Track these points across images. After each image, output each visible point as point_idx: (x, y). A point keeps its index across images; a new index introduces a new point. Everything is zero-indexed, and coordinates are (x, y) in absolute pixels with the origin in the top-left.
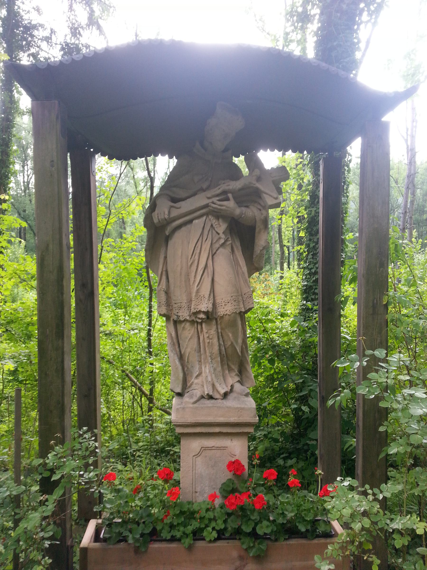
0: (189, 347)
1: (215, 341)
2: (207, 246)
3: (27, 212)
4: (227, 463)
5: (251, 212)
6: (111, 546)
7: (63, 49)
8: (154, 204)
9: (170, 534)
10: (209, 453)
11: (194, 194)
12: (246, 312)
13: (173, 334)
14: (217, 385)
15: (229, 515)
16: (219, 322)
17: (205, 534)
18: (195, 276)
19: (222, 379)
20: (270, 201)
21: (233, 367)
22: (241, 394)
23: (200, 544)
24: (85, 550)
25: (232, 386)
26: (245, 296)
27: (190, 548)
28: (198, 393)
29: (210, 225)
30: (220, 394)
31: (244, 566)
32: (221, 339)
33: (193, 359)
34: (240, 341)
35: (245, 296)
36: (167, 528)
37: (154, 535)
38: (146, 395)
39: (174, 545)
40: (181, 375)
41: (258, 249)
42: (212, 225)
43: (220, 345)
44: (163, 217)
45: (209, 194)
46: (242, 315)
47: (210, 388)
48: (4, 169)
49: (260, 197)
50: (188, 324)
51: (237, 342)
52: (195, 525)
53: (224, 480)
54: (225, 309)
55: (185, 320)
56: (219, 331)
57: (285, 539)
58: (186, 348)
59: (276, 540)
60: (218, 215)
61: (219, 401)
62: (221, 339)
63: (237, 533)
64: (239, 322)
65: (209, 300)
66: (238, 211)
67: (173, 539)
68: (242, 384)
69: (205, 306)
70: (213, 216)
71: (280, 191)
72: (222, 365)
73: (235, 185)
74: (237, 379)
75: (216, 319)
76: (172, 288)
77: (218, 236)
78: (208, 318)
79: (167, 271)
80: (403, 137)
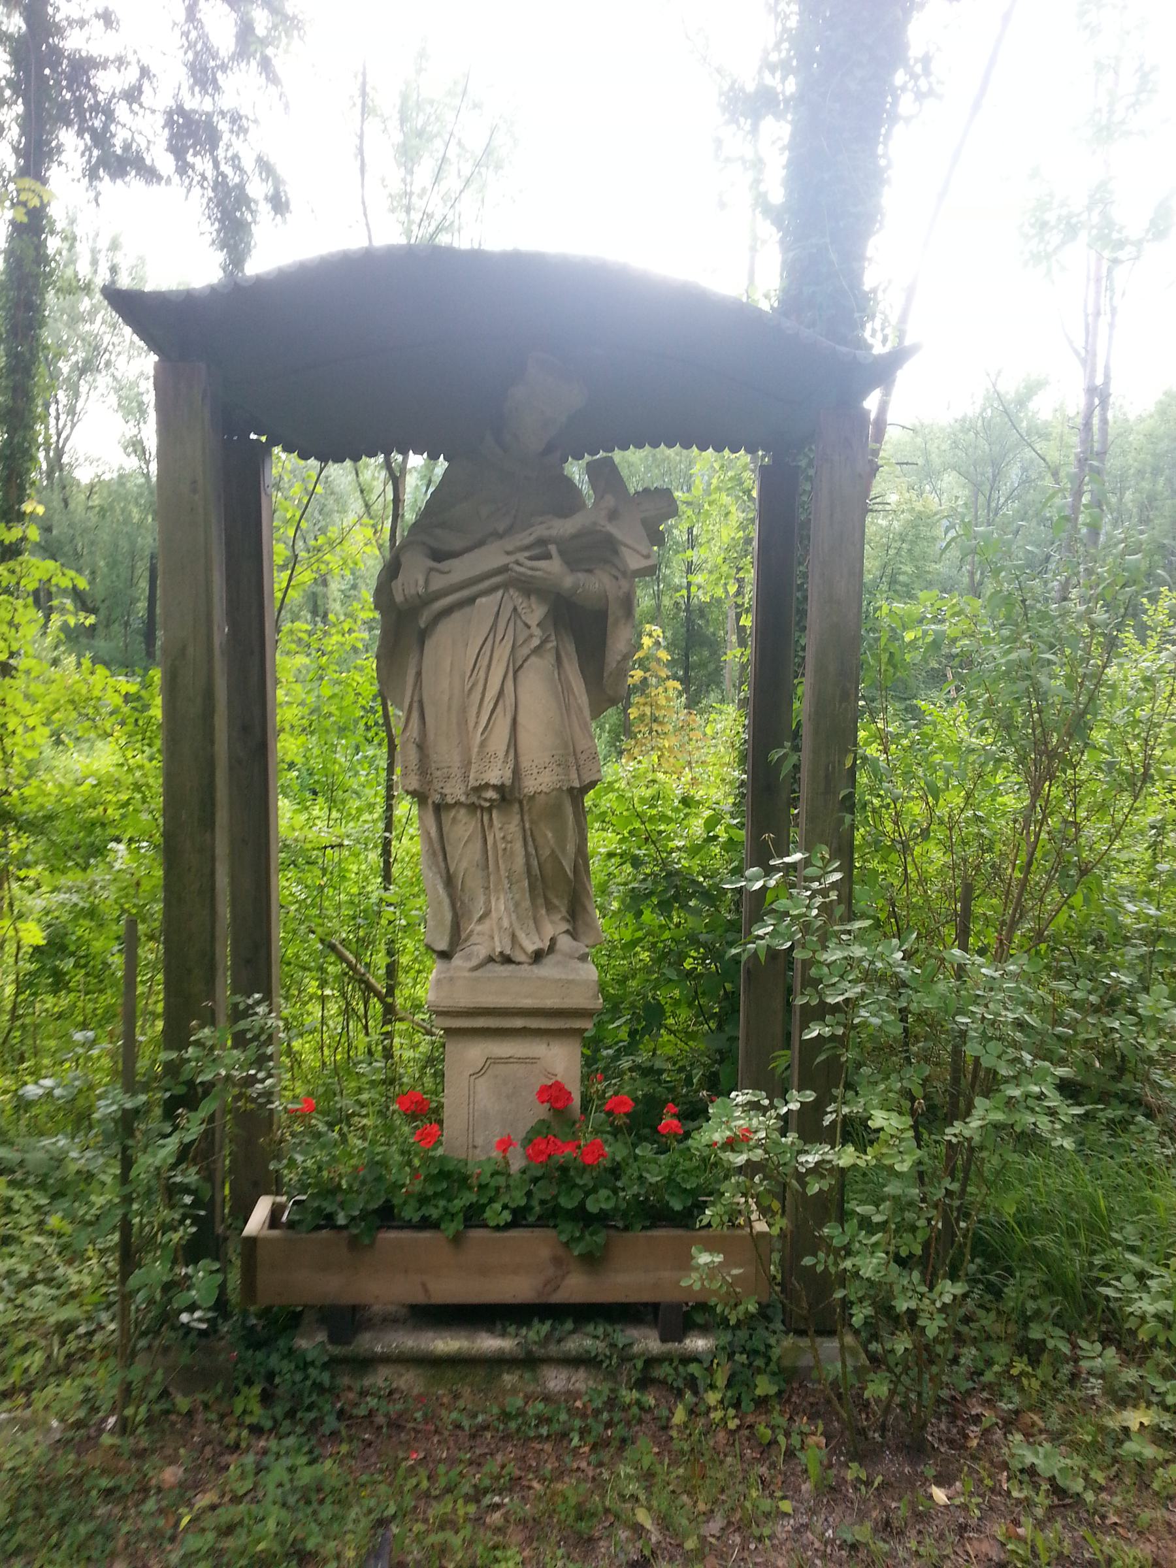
0: (465, 859)
1: (518, 846)
2: (503, 653)
3: (55, 532)
4: (537, 1089)
5: (596, 583)
6: (304, 1235)
7: (170, 123)
8: (392, 569)
9: (420, 1214)
10: (501, 1069)
11: (480, 544)
12: (585, 789)
13: (433, 832)
14: (521, 936)
15: (535, 1180)
16: (526, 808)
17: (488, 1214)
18: (478, 713)
19: (532, 925)
20: (634, 563)
21: (556, 902)
22: (571, 957)
23: (477, 1234)
24: (252, 1241)
25: (553, 940)
26: (583, 757)
27: (457, 1240)
28: (482, 952)
29: (510, 608)
30: (525, 952)
31: (563, 1277)
32: (530, 843)
33: (474, 883)
34: (571, 848)
35: (583, 757)
36: (413, 1203)
37: (386, 1216)
38: (377, 994)
39: (426, 1235)
40: (448, 916)
41: (612, 659)
42: (515, 609)
43: (527, 855)
44: (413, 592)
45: (510, 544)
46: (577, 794)
47: (507, 941)
48: (21, 433)
49: (616, 552)
50: (463, 811)
51: (563, 850)
52: (470, 1197)
53: (531, 1121)
54: (540, 780)
55: (458, 804)
56: (527, 826)
57: (644, 1228)
58: (460, 861)
59: (626, 1228)
60: (528, 587)
61: (525, 966)
62: (530, 843)
63: (551, 1216)
64: (569, 810)
65: (505, 762)
66: (568, 581)
67: (426, 1224)
68: (575, 939)
69: (497, 774)
70: (519, 589)
71: (658, 538)
72: (533, 899)
73: (565, 527)
74: (565, 926)
75: (521, 802)
76: (431, 736)
77: (526, 633)
78: (503, 799)
79: (421, 702)
80: (1077, 353)
